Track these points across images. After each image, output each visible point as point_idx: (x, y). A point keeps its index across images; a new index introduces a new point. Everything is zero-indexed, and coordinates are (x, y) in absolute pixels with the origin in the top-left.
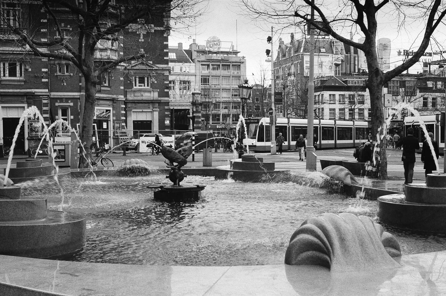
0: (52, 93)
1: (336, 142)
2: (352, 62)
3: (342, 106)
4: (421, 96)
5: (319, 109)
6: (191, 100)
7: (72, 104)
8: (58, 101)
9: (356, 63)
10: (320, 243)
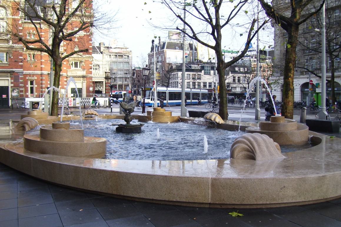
0: (25, 72)
1: (191, 101)
2: (194, 55)
3: (189, 81)
4: (232, 76)
5: (175, 82)
6: (105, 76)
7: (36, 78)
8: (28, 76)
9: (196, 56)
10: (248, 147)
